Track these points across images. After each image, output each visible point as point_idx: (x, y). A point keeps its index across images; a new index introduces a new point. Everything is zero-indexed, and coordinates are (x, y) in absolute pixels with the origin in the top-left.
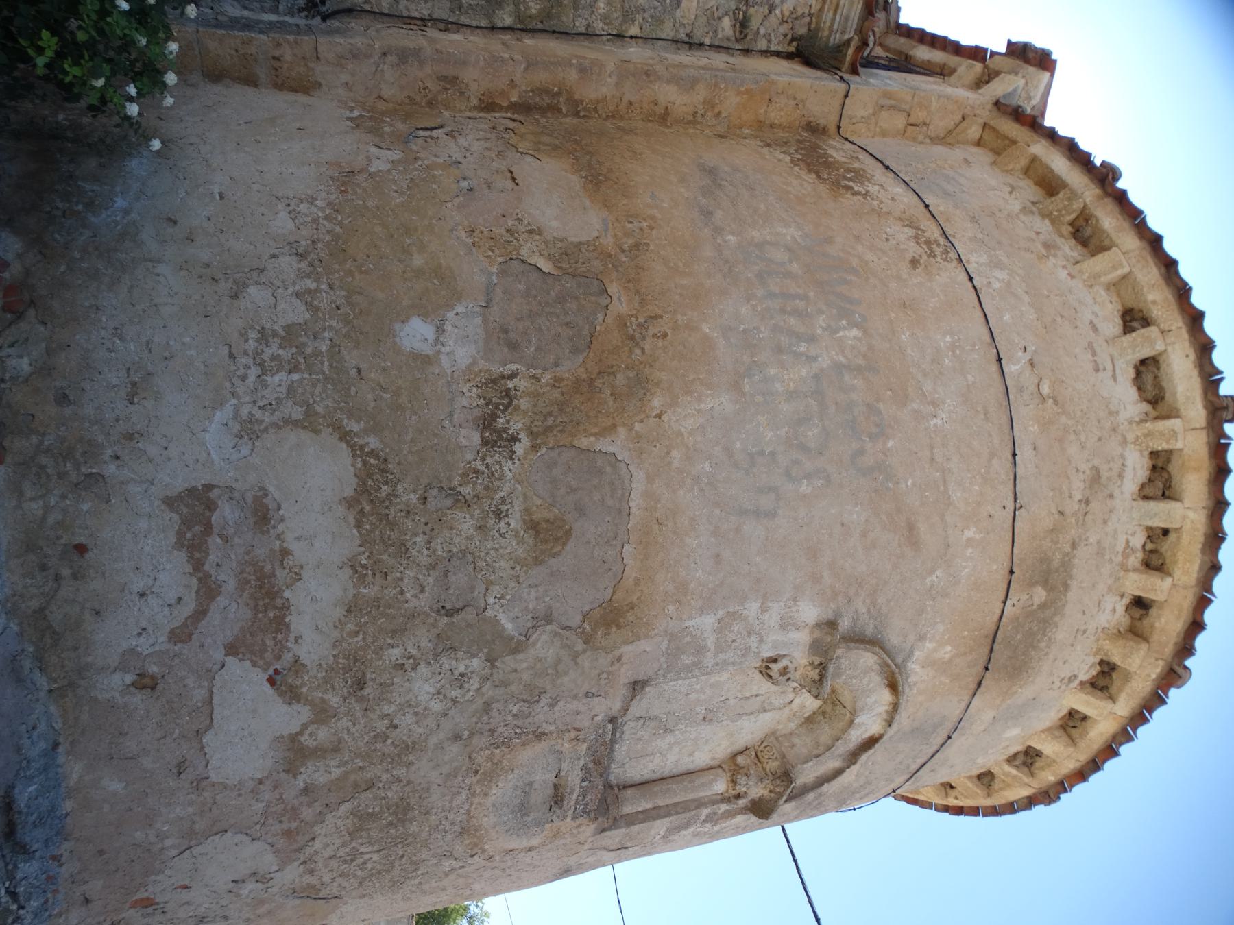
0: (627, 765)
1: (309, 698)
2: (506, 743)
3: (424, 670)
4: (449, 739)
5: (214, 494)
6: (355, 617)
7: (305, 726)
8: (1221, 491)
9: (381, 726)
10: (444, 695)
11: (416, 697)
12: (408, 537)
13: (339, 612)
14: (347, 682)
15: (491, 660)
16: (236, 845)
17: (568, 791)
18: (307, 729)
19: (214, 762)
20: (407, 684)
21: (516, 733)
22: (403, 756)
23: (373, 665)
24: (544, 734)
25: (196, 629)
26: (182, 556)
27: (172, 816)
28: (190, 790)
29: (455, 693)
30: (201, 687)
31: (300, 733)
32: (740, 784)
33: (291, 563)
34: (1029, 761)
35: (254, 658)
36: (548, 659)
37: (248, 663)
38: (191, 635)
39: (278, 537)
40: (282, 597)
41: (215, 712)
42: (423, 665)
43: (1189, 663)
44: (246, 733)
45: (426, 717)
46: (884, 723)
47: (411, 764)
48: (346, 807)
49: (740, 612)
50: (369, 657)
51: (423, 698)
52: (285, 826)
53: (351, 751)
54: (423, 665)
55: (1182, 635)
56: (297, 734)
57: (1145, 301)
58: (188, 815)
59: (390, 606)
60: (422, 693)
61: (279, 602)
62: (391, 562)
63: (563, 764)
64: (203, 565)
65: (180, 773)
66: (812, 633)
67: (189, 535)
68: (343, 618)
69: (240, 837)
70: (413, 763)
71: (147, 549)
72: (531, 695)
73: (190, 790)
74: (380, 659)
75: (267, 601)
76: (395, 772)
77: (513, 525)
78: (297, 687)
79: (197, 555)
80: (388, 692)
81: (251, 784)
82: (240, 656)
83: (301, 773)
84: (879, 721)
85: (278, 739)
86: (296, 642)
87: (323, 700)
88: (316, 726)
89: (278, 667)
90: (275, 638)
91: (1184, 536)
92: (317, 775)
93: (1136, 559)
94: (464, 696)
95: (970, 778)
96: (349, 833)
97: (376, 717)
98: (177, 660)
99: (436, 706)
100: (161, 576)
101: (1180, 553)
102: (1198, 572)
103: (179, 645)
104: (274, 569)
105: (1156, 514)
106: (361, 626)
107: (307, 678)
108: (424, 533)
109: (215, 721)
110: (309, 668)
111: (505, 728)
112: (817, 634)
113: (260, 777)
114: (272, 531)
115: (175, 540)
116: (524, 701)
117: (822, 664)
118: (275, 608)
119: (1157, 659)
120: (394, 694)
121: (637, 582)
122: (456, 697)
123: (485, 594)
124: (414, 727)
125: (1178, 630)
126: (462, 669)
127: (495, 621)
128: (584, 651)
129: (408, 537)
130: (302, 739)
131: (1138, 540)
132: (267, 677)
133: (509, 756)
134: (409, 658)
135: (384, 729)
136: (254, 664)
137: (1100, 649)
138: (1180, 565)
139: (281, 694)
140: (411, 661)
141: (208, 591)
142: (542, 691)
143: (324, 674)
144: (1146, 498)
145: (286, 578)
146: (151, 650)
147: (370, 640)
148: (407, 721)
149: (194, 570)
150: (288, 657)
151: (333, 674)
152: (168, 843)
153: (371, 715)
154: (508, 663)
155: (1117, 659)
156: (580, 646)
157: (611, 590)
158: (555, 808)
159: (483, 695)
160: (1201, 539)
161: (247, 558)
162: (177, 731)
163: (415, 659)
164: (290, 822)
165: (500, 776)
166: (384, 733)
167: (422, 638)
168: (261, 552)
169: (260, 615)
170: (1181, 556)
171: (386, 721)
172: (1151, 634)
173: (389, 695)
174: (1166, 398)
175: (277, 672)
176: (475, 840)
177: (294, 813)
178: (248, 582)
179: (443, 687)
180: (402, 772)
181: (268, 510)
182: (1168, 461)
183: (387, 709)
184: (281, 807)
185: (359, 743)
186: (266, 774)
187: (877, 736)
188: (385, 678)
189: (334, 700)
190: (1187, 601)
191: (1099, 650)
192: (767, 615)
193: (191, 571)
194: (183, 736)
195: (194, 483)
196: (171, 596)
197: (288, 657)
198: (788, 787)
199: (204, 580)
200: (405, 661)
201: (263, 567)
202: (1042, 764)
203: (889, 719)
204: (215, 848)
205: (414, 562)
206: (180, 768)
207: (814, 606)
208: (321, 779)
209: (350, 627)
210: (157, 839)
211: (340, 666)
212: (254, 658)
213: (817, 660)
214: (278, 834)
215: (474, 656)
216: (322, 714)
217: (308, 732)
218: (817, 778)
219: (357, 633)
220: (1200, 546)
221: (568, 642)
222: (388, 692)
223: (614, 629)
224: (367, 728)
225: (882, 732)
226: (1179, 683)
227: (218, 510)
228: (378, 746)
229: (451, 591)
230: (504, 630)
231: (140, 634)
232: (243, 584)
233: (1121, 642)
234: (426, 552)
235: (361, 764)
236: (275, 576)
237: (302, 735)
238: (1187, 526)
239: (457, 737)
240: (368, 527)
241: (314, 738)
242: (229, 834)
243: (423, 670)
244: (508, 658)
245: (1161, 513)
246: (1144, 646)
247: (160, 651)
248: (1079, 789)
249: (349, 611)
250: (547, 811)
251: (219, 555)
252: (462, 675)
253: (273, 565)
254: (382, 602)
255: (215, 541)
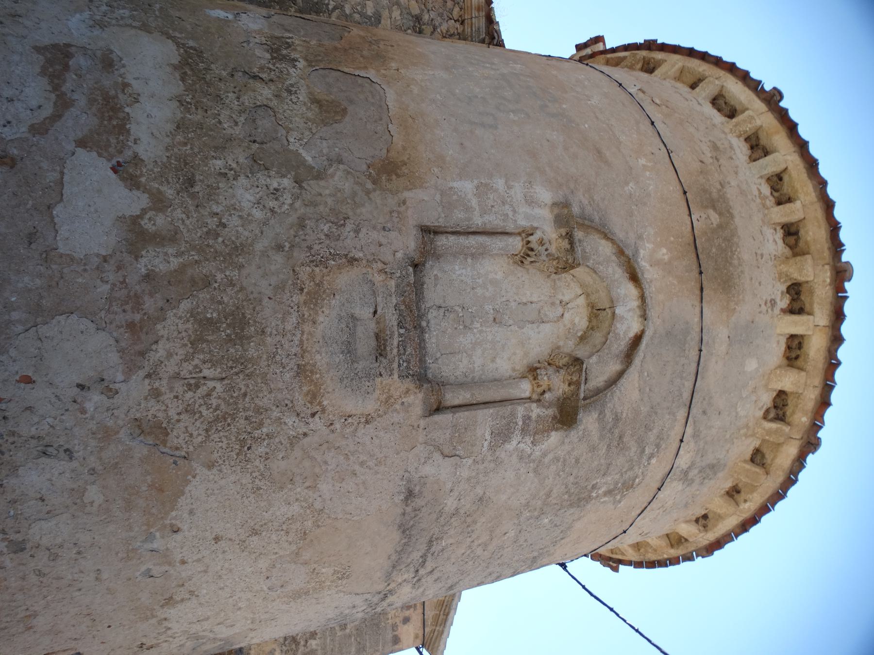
0: (440, 361)
1: (148, 187)
2: (322, 263)
3: (244, 181)
4: (272, 248)
5: (73, 50)
6: (183, 132)
7: (144, 211)
8: (799, 136)
9: (212, 223)
10: (264, 206)
11: (240, 202)
12: (222, 93)
13: (170, 127)
14: (179, 179)
15: (298, 182)
16: (82, 332)
17: (388, 333)
18: (146, 213)
19: (63, 232)
20: (230, 190)
21: (330, 253)
22: (234, 257)
23: (201, 168)
24: (356, 260)
25: (53, 126)
26: (44, 82)
27: (20, 285)
28: (39, 262)
29: (272, 204)
30: (54, 170)
31: (141, 216)
32: (541, 375)
33: (130, 91)
34: (781, 413)
35: (100, 151)
36: (346, 191)
37: (94, 154)
38: (47, 131)
39: (121, 76)
40: (124, 112)
41: (65, 187)
42: (242, 177)
43: (845, 258)
44: (92, 209)
45: (250, 222)
46: (640, 320)
47: (242, 266)
48: (185, 305)
49: (491, 185)
50: (197, 162)
51: (246, 205)
52: (129, 317)
53: (187, 242)
54: (242, 177)
55: (829, 240)
56: (138, 217)
57: (699, 73)
58: (37, 288)
59: (211, 130)
60: (244, 200)
61: (121, 115)
62: (209, 104)
63: (378, 299)
64: (61, 87)
65: (31, 243)
66: (552, 211)
67: (50, 70)
68: (173, 131)
69: (85, 323)
70: (243, 266)
71: (17, 72)
72: (337, 218)
73: (39, 262)
74: (206, 166)
75: (111, 113)
76: (227, 273)
77: (301, 99)
78: (136, 176)
79: (56, 81)
80: (215, 194)
81: (96, 261)
82: (88, 149)
83: (142, 256)
84: (636, 319)
85: (121, 219)
86: (135, 143)
87: (160, 192)
88: (154, 212)
89: (121, 160)
90: (117, 138)
91: (793, 172)
92: (157, 261)
93: (770, 201)
94: (280, 207)
95: (745, 461)
96: (191, 343)
97: (206, 213)
98: (34, 148)
99: (258, 214)
100: (27, 90)
101: (796, 183)
102: (815, 191)
103: (38, 137)
104: (117, 93)
105: (767, 165)
106: (188, 140)
107: (145, 171)
108: (234, 92)
109: (65, 196)
110: (146, 163)
111: (320, 246)
112: (556, 211)
113: (104, 254)
114: (116, 72)
115: (40, 70)
116: (332, 223)
117: (567, 234)
118: (118, 118)
119: (823, 266)
120: (221, 197)
121: (404, 148)
122: (274, 208)
123: (287, 136)
124: (240, 229)
125: (825, 236)
126: (275, 185)
127: (297, 154)
128: (374, 190)
129: (222, 93)
130: (142, 223)
131: (766, 190)
132: (110, 166)
133: (328, 278)
134: (231, 170)
135: (214, 227)
136: (100, 155)
137: (781, 273)
138: (800, 191)
139: (123, 179)
140: (232, 172)
141: (63, 104)
142: (346, 216)
143: (159, 170)
144: (755, 160)
145: (126, 100)
146: (13, 137)
147: (196, 150)
148: (234, 221)
149: (53, 88)
150: (128, 153)
151: (167, 170)
152: (15, 315)
153: (202, 211)
154: (313, 186)
155: (796, 275)
156: (369, 185)
157: (386, 151)
158: (381, 358)
159: (296, 210)
160: (804, 170)
161: (95, 86)
162: (30, 202)
163: (235, 172)
164: (133, 312)
165: (324, 299)
166: (215, 230)
167: (239, 156)
168: (107, 83)
169: (106, 122)
170: (798, 185)
171: (215, 219)
172: (808, 247)
173: (216, 197)
174: (738, 109)
175: (118, 163)
176: (312, 387)
177: (136, 302)
178: (96, 100)
179: (261, 198)
180: (234, 274)
181: (113, 61)
182: (758, 138)
183: (216, 209)
184: (124, 292)
185: (193, 235)
186: (110, 252)
187: (639, 333)
188: (211, 181)
189: (169, 192)
190: (817, 212)
191: (780, 274)
192: (512, 192)
193: (51, 89)
194: (35, 208)
195: (57, 42)
196: (34, 103)
197: (128, 153)
198: (581, 370)
199: (61, 96)
200: (227, 171)
201: (108, 92)
202: (791, 410)
203: (642, 313)
204: (61, 332)
205: (227, 106)
206: (31, 238)
207: (547, 190)
208: (162, 267)
209: (179, 138)
210: (4, 310)
211: (173, 166)
212: (100, 151)
213: (563, 231)
214: (122, 327)
215: (283, 176)
216: (159, 203)
217: (147, 216)
218: (606, 382)
219: (185, 144)
220: (806, 175)
221: (360, 181)
222: (215, 194)
223: (394, 177)
224: (200, 222)
225: (642, 328)
226: (848, 274)
227: (74, 58)
228: (211, 242)
229: (260, 130)
230: (306, 161)
231: (5, 126)
232: (91, 101)
233: (792, 261)
234: (236, 103)
235: (196, 258)
236: (117, 97)
237: (142, 219)
238: (791, 167)
239: (279, 248)
240: (190, 82)
241: (152, 222)
242: (74, 317)
243: (242, 180)
244: (311, 182)
245: (770, 165)
246: (808, 257)
247: (21, 138)
248: (829, 415)
249: (178, 127)
250: (374, 361)
251: (74, 85)
252: (277, 190)
253: (116, 91)
254: (205, 126)
255: (71, 76)
